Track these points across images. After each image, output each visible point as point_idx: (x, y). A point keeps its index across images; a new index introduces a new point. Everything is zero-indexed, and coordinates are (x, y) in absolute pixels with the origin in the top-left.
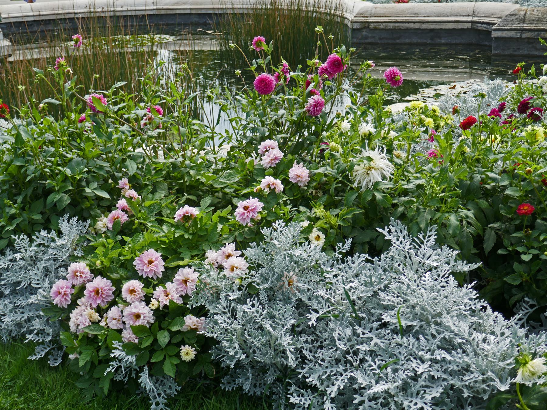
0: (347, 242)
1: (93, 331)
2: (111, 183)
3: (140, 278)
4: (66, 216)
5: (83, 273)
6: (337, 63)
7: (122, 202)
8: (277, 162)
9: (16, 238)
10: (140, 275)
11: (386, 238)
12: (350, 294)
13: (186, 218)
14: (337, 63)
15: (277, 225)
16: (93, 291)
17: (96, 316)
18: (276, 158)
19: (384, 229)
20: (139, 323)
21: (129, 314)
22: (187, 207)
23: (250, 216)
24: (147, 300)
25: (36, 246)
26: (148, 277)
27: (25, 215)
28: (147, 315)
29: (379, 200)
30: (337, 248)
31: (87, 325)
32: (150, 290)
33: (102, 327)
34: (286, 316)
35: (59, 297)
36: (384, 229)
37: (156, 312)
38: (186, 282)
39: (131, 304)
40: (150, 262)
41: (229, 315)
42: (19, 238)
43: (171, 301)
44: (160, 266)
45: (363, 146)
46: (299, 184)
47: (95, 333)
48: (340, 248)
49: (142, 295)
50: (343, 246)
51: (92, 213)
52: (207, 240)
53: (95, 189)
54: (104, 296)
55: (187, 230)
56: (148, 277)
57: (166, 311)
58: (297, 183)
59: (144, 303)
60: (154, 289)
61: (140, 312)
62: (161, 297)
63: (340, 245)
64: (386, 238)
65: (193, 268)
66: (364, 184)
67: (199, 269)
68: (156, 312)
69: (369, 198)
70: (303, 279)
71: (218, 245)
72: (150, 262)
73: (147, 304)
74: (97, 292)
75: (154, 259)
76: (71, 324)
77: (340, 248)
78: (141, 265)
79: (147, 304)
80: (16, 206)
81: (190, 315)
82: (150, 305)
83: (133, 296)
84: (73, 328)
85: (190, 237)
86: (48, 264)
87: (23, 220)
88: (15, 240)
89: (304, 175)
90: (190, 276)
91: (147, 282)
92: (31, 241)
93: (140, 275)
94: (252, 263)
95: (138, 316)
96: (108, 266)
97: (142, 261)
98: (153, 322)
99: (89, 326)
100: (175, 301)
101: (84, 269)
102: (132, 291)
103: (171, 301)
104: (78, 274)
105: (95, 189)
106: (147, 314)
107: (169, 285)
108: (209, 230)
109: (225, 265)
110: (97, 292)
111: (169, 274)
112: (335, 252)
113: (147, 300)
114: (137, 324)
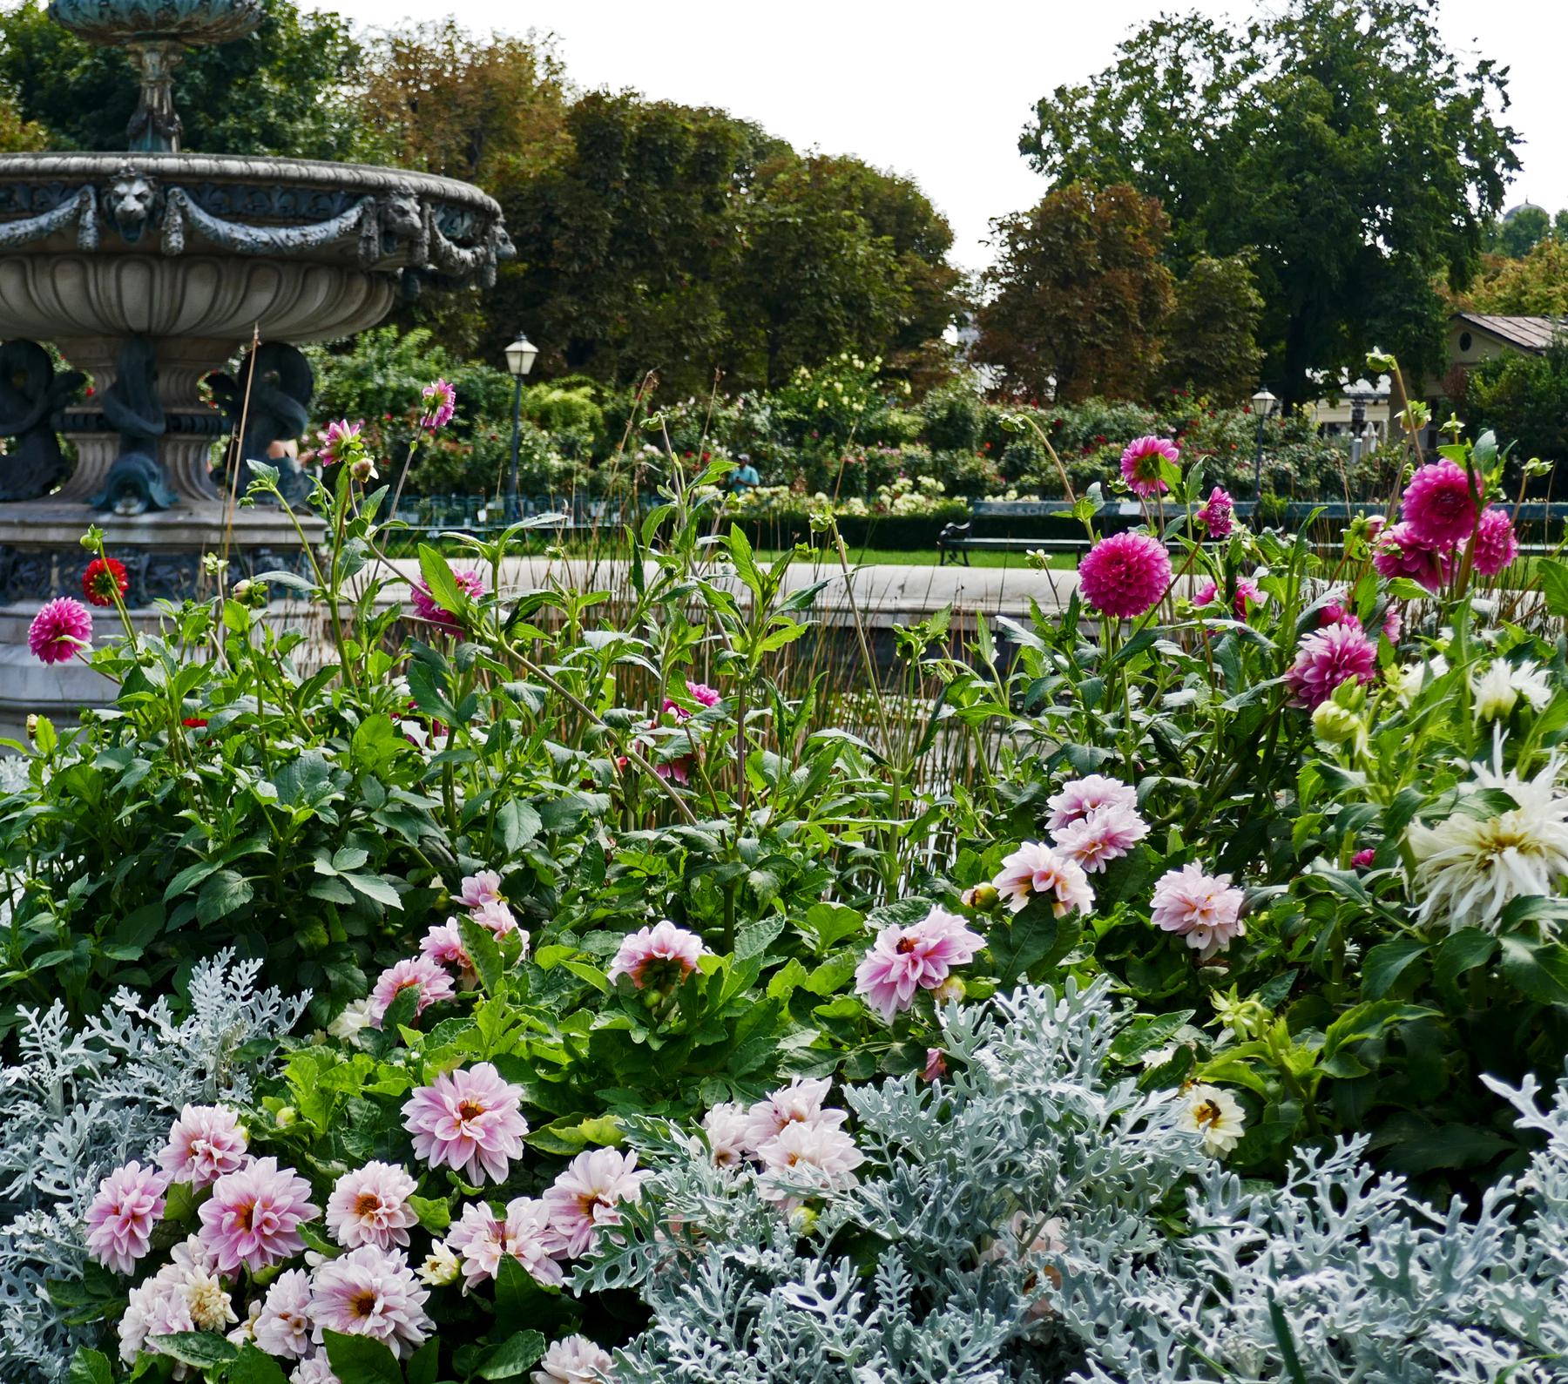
0: (1342, 1149)
1: (194, 1355)
2: (438, 891)
3: (416, 1169)
4: (226, 955)
5: (218, 1145)
6: (1449, 499)
7: (447, 934)
8: (1114, 853)
9: (32, 1017)
10: (418, 1156)
11: (1520, 1123)
12: (1295, 1324)
13: (659, 970)
14: (1449, 499)
15: (1013, 1005)
16: (235, 1208)
17: (221, 1305)
18: (1110, 840)
19: (1518, 1085)
20: (365, 1327)
21: (335, 1292)
22: (666, 928)
23: (915, 976)
24: (418, 1246)
25: (88, 1044)
26: (444, 1167)
27: (87, 945)
28: (401, 1301)
29: (1518, 968)
30: (1293, 1171)
31: (177, 1327)
32: (443, 1206)
33: (231, 1346)
34: (967, 1355)
35: (112, 1223)
36: (1518, 1085)
37: (443, 1299)
38: (589, 1203)
39: (345, 1249)
40: (468, 1112)
41: (727, 1333)
42: (39, 1019)
43: (510, 1264)
44: (509, 1140)
45: (1484, 754)
46: (1193, 942)
47: (198, 1364)
48: (1305, 1171)
49: (402, 1223)
50: (1319, 1162)
51: (334, 976)
52: (725, 1070)
53: (357, 872)
54: (268, 1232)
55: (647, 1018)
56: (444, 1167)
57: (486, 1305)
58: (1180, 936)
59: (399, 1258)
60: (457, 1214)
61: (377, 1282)
62: (472, 1246)
63: (1309, 1155)
64: (1520, 1123)
65: (633, 1157)
66: (1463, 907)
67: (659, 1156)
68: (443, 1299)
69: (1475, 962)
70: (1090, 1241)
71: (758, 1080)
72: (468, 1112)
73: (415, 1261)
74: (245, 1216)
75: (487, 1103)
76: (125, 1329)
77: (1305, 1171)
78: (428, 1116)
79: (415, 1261)
80: (60, 904)
81: (580, 1341)
82: (424, 1270)
83: (364, 1221)
84: (127, 1349)
85: (656, 1046)
86: (113, 1118)
87: (78, 960)
88: (26, 1022)
89: (1217, 903)
90: (611, 1180)
91: (435, 1182)
92: (76, 1024)
93: (418, 1156)
94: (875, 1154)
95: (364, 1305)
96: (320, 1132)
97: (437, 1101)
98: (419, 1337)
99: (184, 1335)
100: (529, 1268)
101: (227, 1129)
102: (367, 1205)
103: (510, 1264)
104: (200, 1145)
105: (357, 872)
106: (402, 1298)
107: (520, 1207)
108: (741, 1027)
109: (766, 1153)
110: (245, 1216)
111: (534, 1172)
112: (1283, 1183)
113: (418, 1246)
114: (354, 1330)
